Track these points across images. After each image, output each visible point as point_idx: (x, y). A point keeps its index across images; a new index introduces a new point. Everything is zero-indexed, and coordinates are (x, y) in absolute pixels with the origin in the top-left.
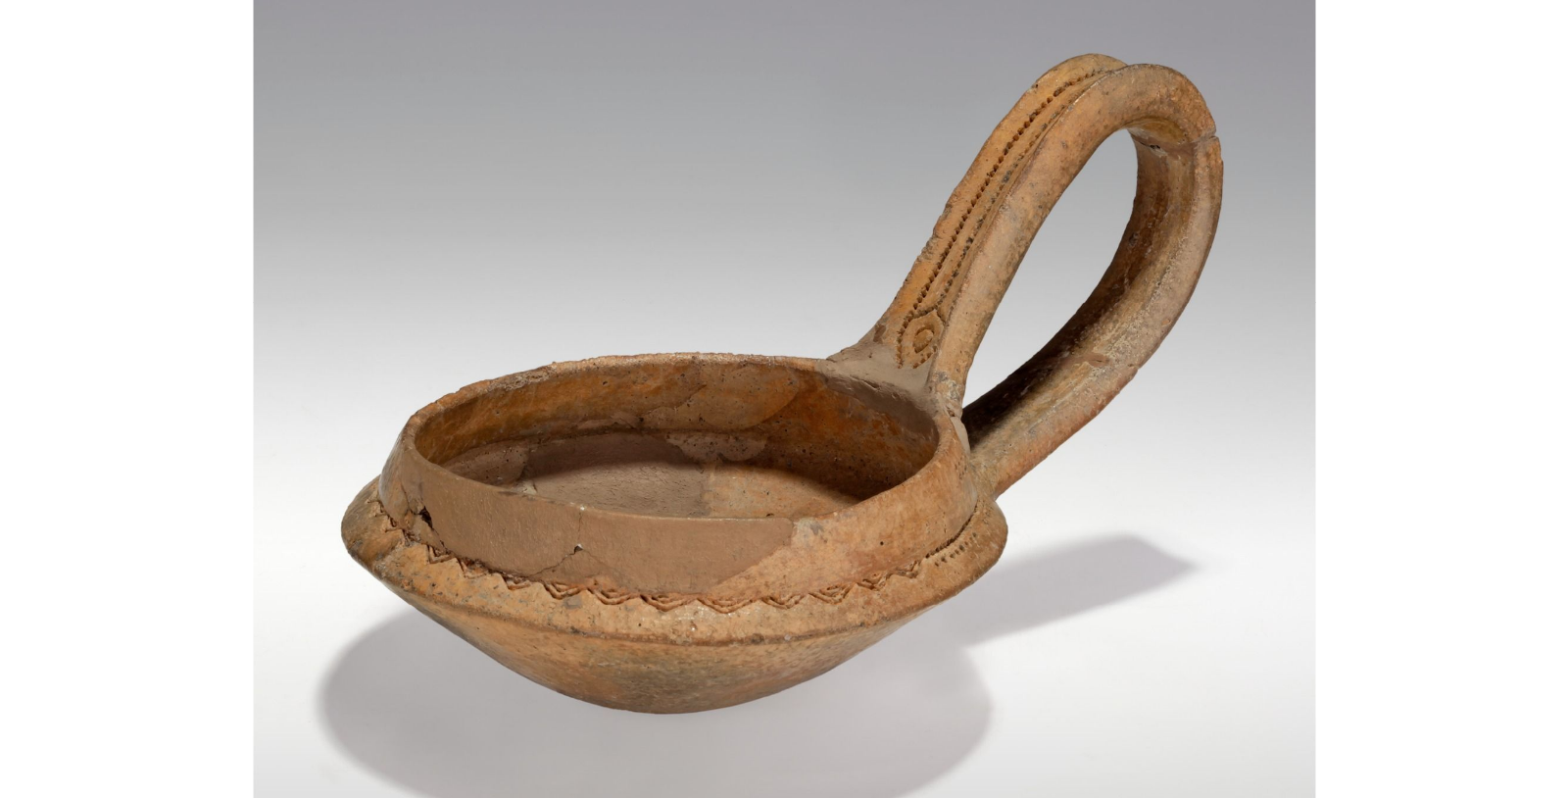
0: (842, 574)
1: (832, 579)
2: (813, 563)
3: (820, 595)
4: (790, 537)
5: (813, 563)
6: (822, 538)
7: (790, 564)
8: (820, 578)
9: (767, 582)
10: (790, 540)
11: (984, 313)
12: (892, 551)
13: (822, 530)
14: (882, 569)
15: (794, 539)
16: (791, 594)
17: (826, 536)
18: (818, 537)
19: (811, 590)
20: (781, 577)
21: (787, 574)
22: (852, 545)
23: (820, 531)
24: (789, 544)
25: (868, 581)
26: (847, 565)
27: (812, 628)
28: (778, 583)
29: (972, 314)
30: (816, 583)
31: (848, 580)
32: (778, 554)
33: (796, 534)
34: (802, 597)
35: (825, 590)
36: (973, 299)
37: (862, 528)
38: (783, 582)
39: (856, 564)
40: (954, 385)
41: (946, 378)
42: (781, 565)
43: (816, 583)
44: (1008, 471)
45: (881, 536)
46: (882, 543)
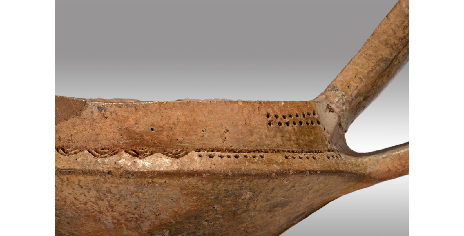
0: (113, 141)
1: (105, 143)
2: (93, 130)
3: (93, 151)
4: (81, 110)
5: (93, 130)
6: (103, 115)
7: (77, 127)
8: (96, 140)
9: (60, 137)
10: (81, 113)
11: (380, 56)
12: (160, 137)
13: (105, 111)
14: (149, 146)
15: (84, 112)
16: (74, 147)
17: (107, 114)
18: (101, 114)
19: (88, 147)
20: (69, 135)
21: (73, 134)
22: (126, 125)
23: (103, 111)
24: (80, 115)
25: (135, 151)
26: (118, 136)
27: (72, 167)
28: (67, 139)
29: (370, 55)
30: (92, 143)
31: (117, 146)
32: (71, 120)
33: (86, 109)
34: (81, 151)
35: (100, 150)
36: (373, 46)
37: (138, 116)
38: (70, 139)
39: (125, 137)
40: (342, 95)
41: (337, 90)
42: (71, 127)
43: (92, 143)
44: (390, 166)
45: (153, 124)
46: (152, 130)
